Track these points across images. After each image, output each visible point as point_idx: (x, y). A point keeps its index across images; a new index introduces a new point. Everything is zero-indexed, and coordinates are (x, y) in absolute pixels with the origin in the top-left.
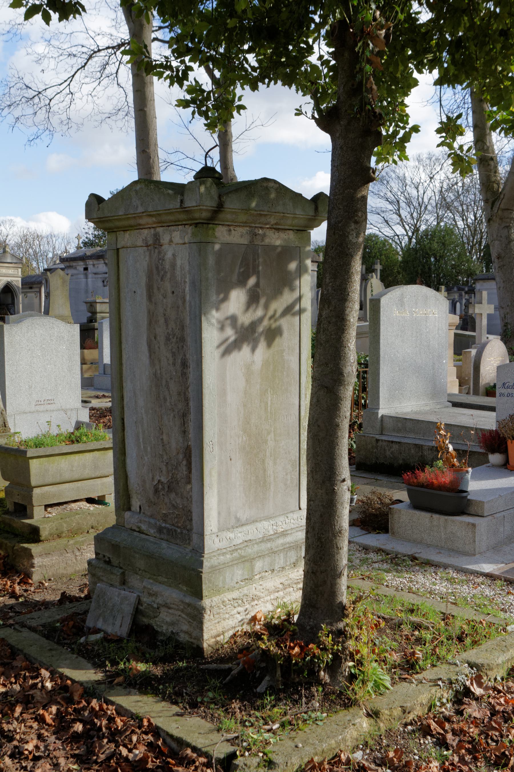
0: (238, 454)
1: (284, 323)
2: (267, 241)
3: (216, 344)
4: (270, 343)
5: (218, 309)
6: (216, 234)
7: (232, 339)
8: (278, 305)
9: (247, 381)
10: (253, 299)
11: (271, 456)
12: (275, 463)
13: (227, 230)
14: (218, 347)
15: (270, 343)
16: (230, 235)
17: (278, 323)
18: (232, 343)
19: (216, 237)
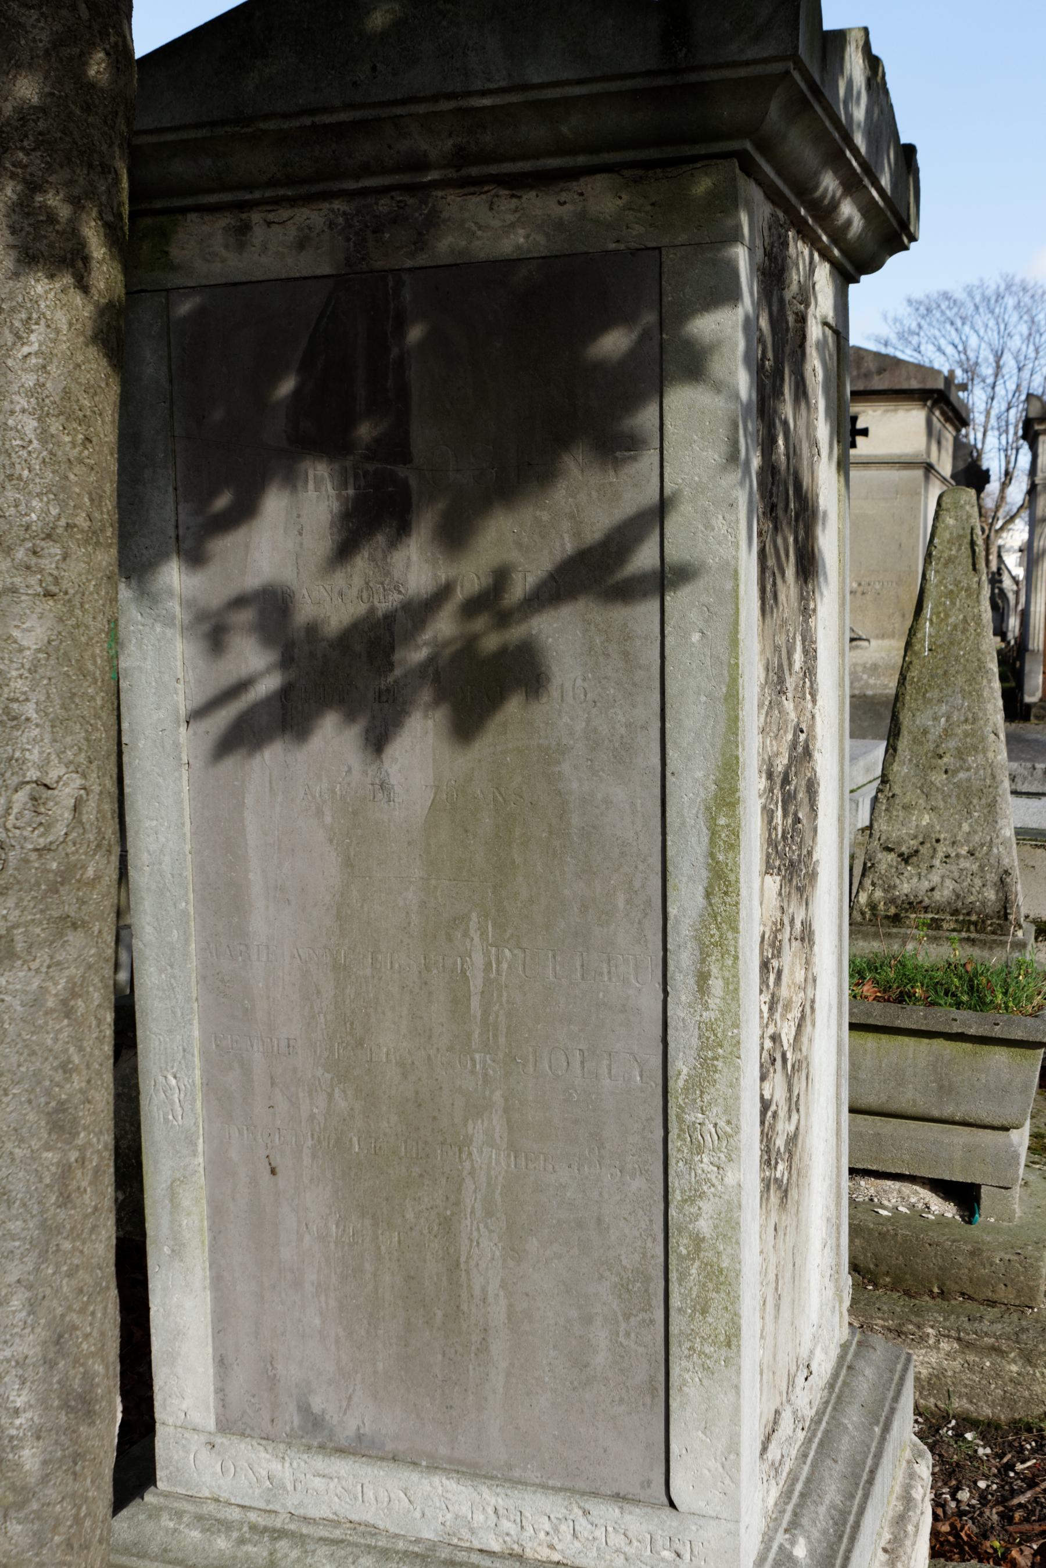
0: (307, 1160)
1: (562, 634)
2: (446, 245)
3: (182, 701)
4: (466, 727)
5: (195, 558)
6: (176, 253)
7: (268, 685)
8: (525, 541)
9: (348, 863)
10: (372, 517)
11: (489, 1214)
12: (514, 1252)
13: (226, 229)
14: (198, 714)
15: (466, 727)
16: (241, 247)
17: (516, 633)
18: (267, 701)
19: (174, 268)
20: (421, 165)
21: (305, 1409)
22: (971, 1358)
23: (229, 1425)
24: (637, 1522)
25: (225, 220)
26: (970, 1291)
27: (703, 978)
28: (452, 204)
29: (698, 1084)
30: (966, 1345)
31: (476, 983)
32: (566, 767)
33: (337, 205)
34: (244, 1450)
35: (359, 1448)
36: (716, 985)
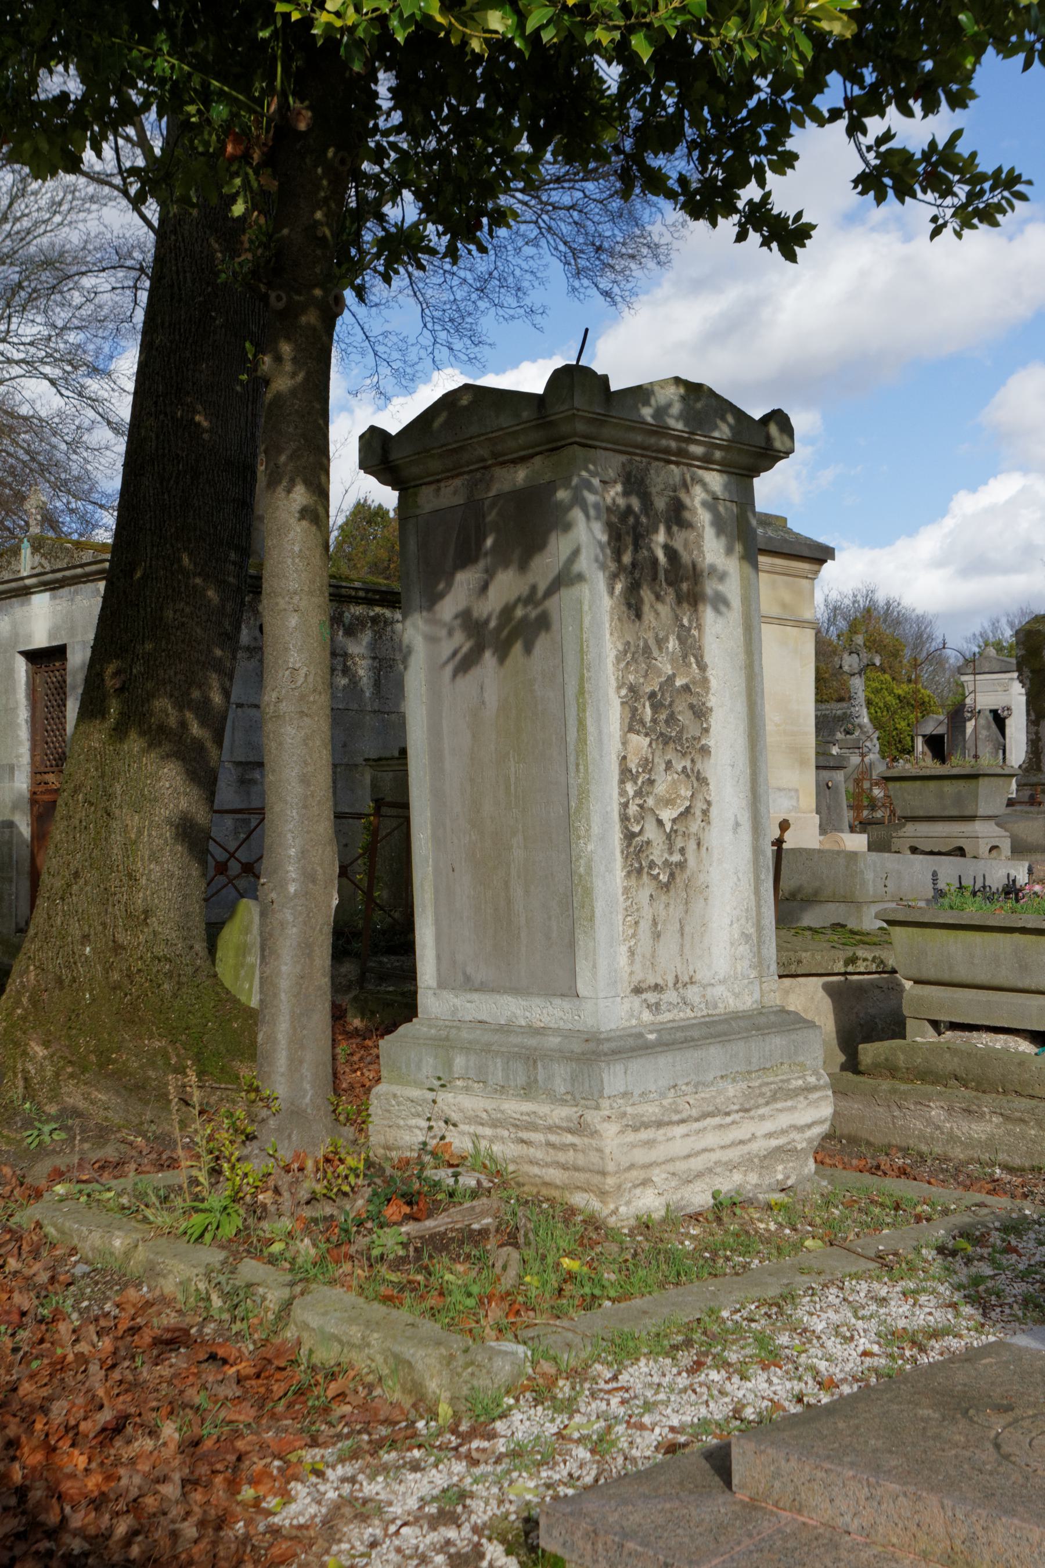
9: (474, 736)
20: (484, 460)
21: (464, 973)
22: (1010, 1127)
23: (442, 985)
24: (566, 1004)
25: (434, 487)
26: (1019, 1089)
27: (578, 765)
28: (499, 472)
29: (578, 809)
30: (1007, 1118)
31: (513, 780)
32: (536, 687)
33: (466, 477)
34: (445, 994)
35: (482, 988)
36: (581, 767)
